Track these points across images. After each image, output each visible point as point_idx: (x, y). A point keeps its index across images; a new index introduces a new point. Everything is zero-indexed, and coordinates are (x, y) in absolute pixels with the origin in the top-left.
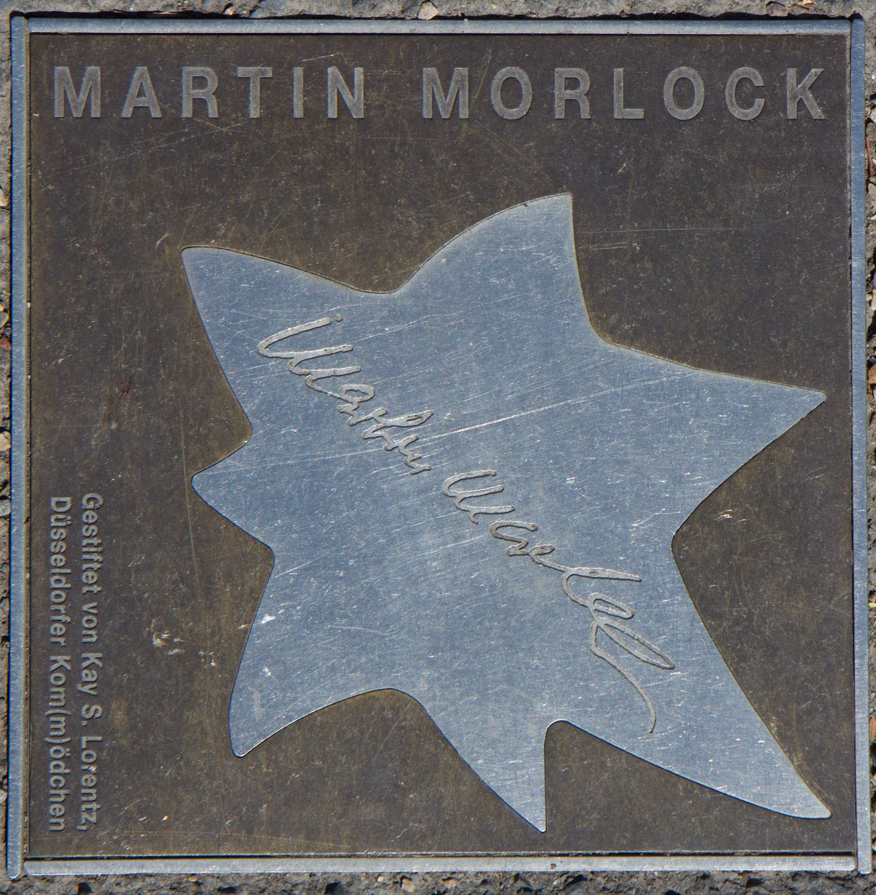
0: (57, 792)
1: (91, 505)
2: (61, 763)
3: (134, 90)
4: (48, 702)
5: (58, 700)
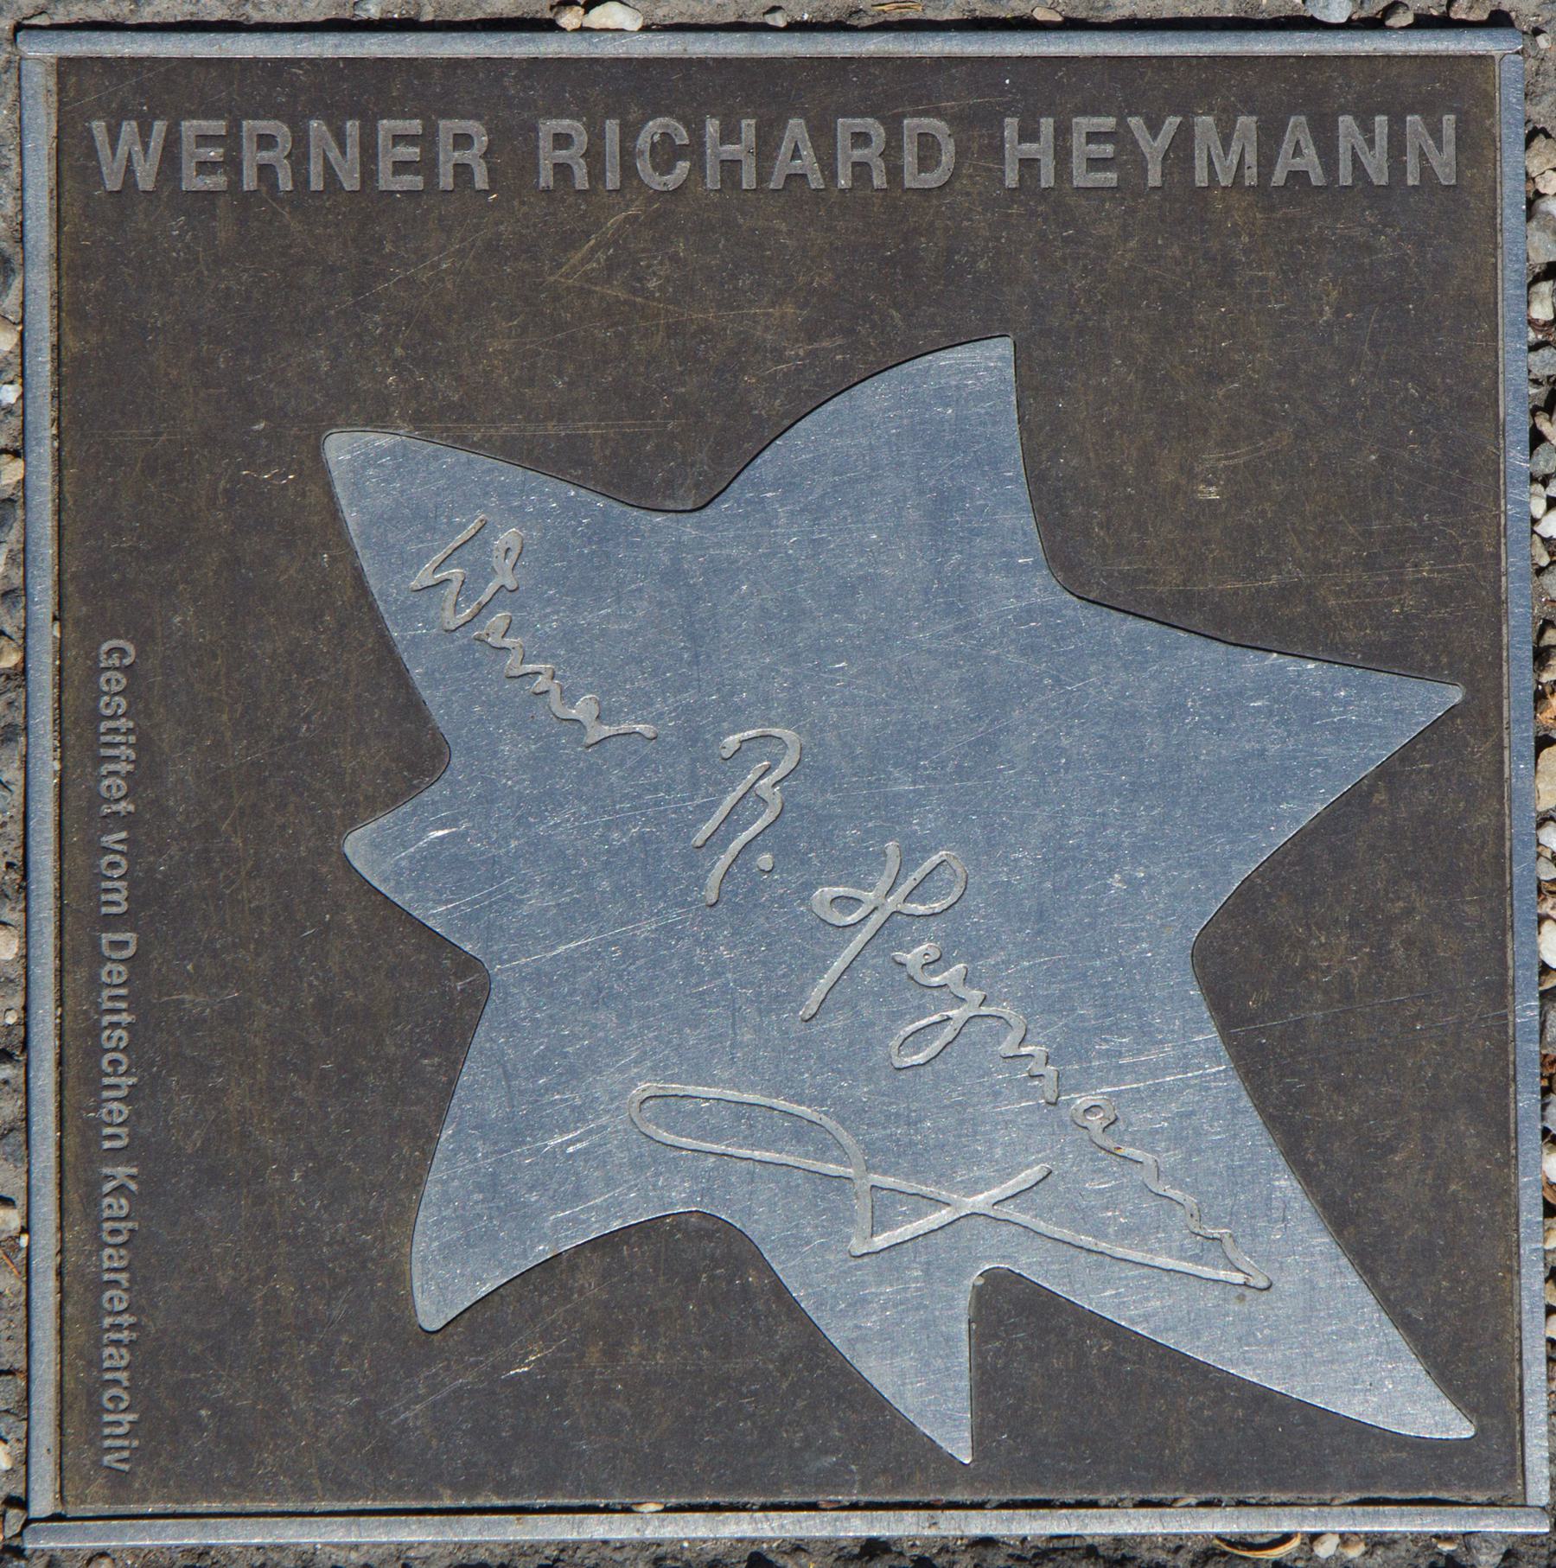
1: (115, 660)
2: (109, 1240)
3: (786, 148)
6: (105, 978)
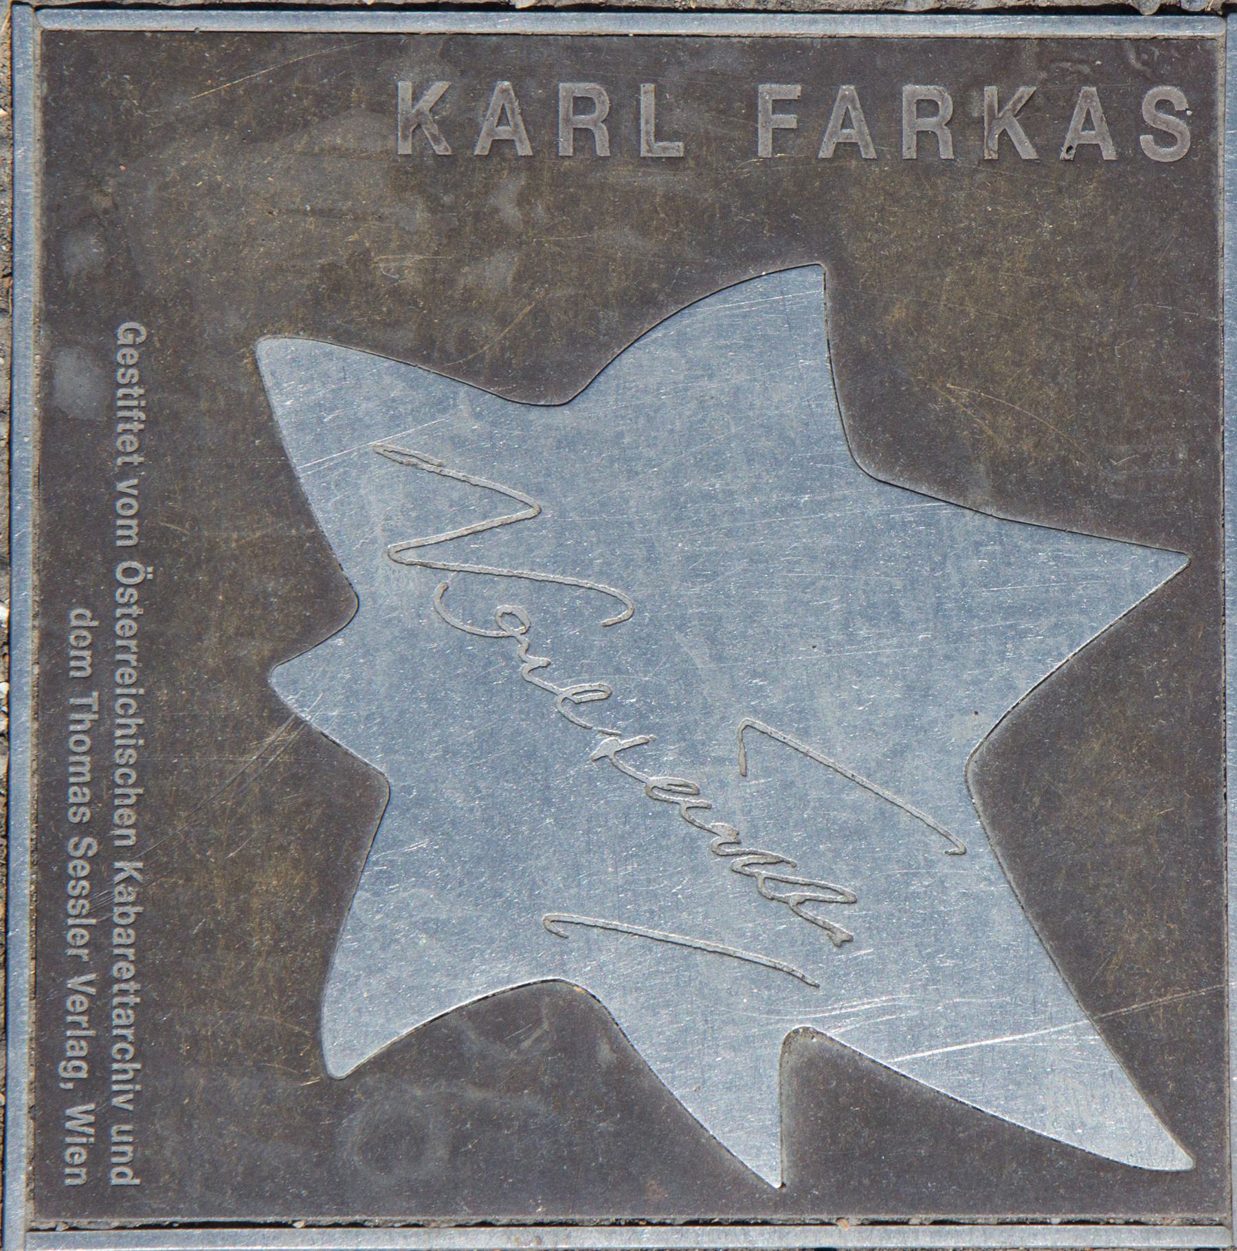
0: (128, 721)
3: (1077, 119)
4: (67, 726)
5: (129, 537)
6: (116, 820)
